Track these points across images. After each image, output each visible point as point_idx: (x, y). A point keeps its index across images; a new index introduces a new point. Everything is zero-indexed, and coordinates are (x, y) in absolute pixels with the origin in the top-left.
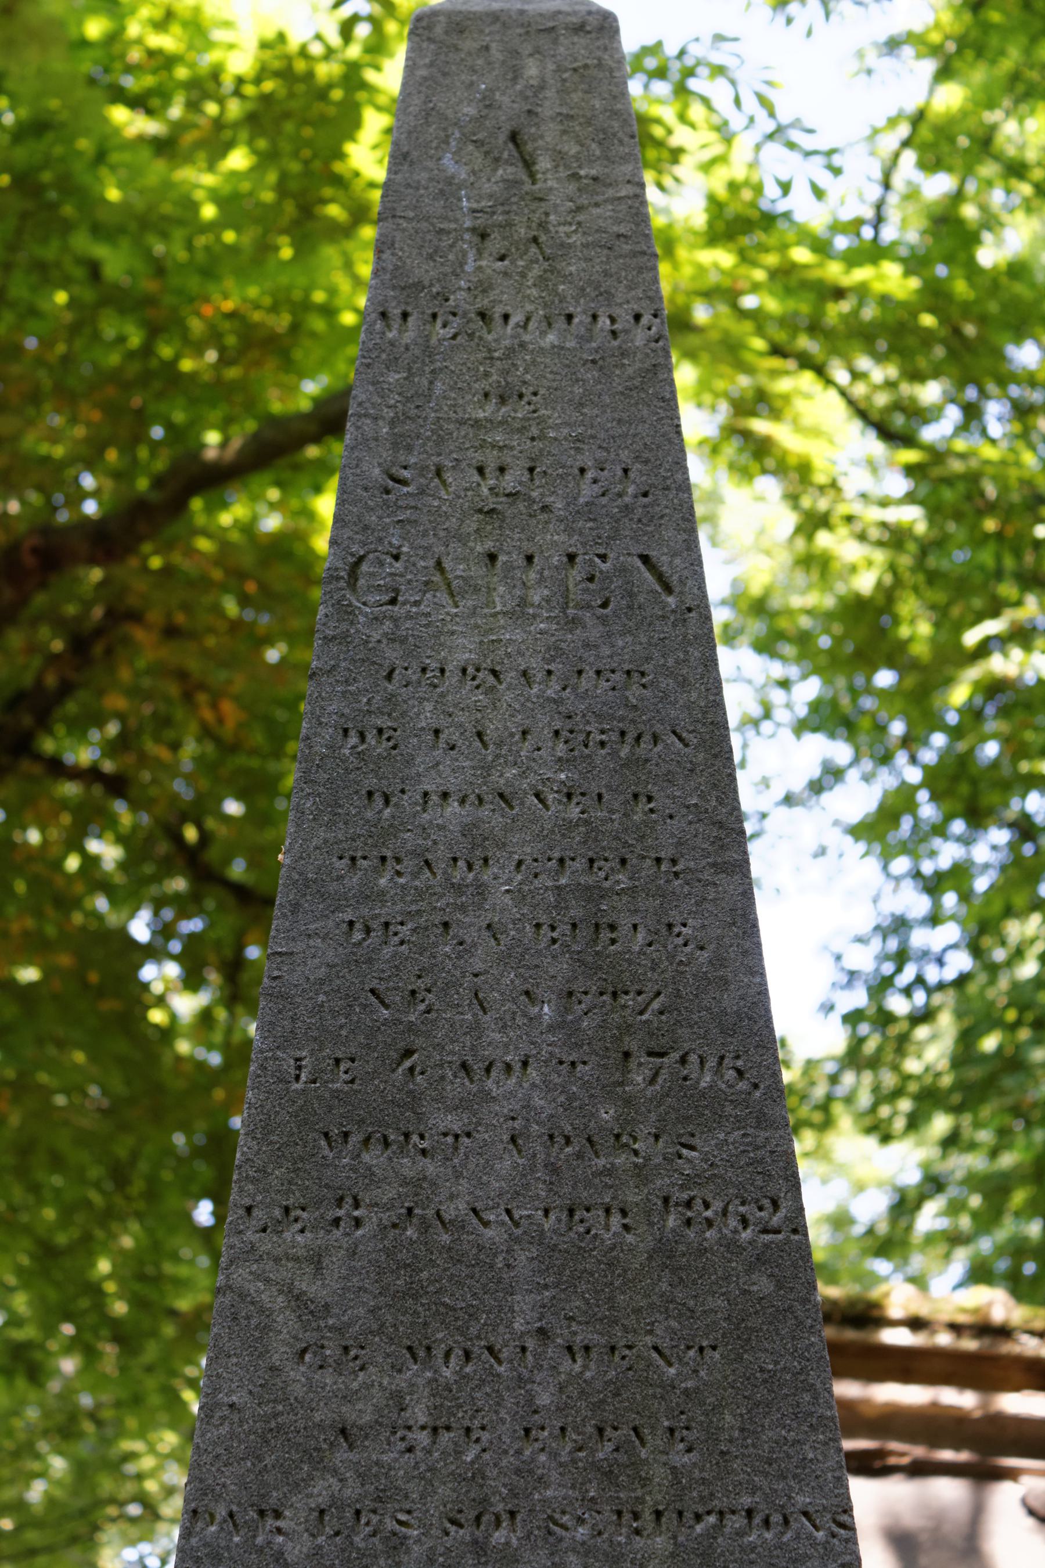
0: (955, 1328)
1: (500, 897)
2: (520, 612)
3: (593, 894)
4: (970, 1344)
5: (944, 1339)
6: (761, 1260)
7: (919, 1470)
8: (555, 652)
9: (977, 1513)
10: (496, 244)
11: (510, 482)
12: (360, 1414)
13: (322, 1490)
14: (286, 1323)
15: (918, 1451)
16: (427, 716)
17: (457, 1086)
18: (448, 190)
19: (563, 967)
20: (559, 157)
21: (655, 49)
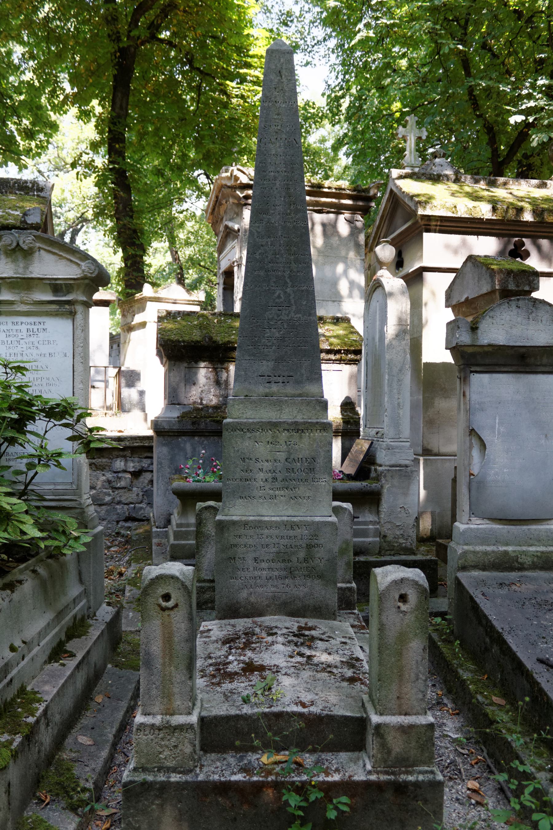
0: (336, 189)
1: (278, 184)
2: (280, 147)
3: (288, 185)
4: (338, 191)
5: (334, 191)
6: (304, 228)
7: (328, 212)
8: (284, 152)
9: (336, 220)
10: (277, 90)
11: (279, 128)
12: (264, 243)
13: (260, 251)
14: (256, 234)
15: (329, 209)
16: (269, 161)
17: (273, 208)
18: (271, 81)
19: (284, 194)
20: (285, 76)
21: (302, 825)
